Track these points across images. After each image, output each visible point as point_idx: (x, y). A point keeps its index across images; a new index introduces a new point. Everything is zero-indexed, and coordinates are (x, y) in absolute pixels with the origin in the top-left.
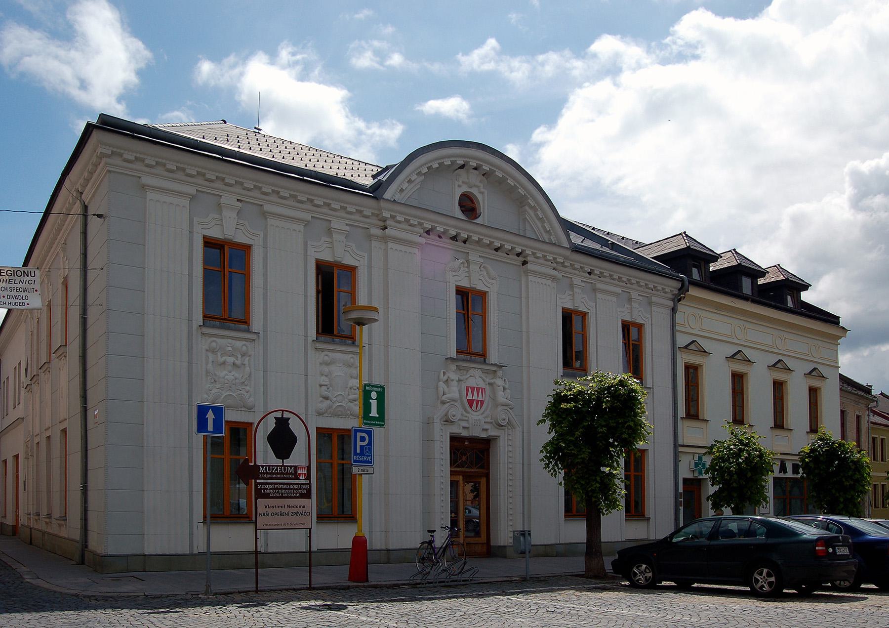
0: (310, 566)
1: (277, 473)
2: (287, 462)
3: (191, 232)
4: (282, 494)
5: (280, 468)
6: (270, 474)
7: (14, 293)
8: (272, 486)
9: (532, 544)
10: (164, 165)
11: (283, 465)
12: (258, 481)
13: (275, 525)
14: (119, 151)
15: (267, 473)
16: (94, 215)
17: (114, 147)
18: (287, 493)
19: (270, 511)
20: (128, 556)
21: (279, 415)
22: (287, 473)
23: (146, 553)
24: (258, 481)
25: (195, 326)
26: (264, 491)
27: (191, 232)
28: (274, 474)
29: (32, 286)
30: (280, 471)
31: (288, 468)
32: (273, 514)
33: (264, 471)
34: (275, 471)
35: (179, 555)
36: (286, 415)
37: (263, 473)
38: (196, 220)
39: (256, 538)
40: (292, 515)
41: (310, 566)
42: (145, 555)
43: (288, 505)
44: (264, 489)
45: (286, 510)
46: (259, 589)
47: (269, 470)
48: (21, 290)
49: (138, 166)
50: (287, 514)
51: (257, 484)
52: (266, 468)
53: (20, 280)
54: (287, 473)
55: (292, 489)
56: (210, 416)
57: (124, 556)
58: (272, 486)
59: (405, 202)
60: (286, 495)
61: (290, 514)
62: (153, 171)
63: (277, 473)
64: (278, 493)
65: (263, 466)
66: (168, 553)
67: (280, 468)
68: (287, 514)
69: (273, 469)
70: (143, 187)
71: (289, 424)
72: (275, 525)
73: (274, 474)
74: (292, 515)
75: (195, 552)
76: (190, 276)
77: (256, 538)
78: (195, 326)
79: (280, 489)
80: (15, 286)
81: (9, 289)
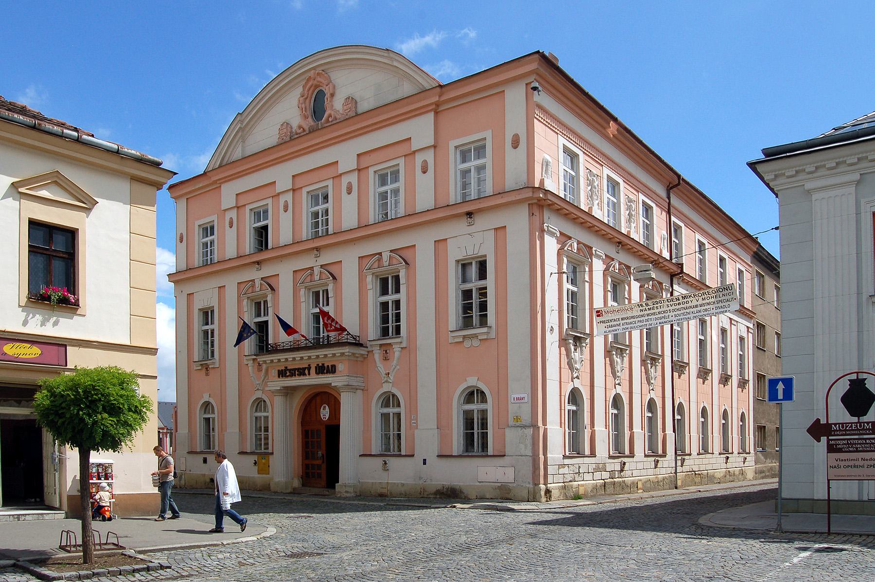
0: (829, 513)
1: (852, 430)
2: (865, 419)
3: (858, 213)
4: (857, 448)
5: (854, 425)
6: (861, 430)
7: (720, 304)
8: (845, 442)
9: (783, 497)
10: (824, 166)
11: (859, 422)
12: (830, 438)
13: (848, 476)
14: (780, 172)
15: (840, 430)
16: (773, 229)
17: (796, 167)
18: (863, 447)
19: (842, 464)
20: (798, 500)
21: (854, 377)
22: (863, 429)
23: (815, 498)
24: (830, 438)
25: (865, 297)
26: (836, 446)
27: (858, 213)
28: (848, 430)
29: (732, 296)
30: (854, 427)
31: (864, 425)
32: (845, 467)
33: (837, 428)
34: (849, 428)
35: (847, 501)
36: (861, 376)
37: (834, 431)
38: (863, 201)
39: (829, 488)
40: (867, 467)
41: (829, 513)
42: (813, 500)
43: (862, 459)
44: (836, 445)
45: (861, 463)
46: (831, 531)
47: (843, 427)
48: (725, 301)
49: (801, 176)
50: (863, 467)
51: (828, 440)
52: (839, 426)
53: (723, 294)
54: (863, 429)
55: (868, 444)
56: (780, 387)
57: (795, 499)
58: (845, 442)
59: (778, 191)
60: (861, 449)
61: (866, 466)
62: (815, 175)
63: (852, 430)
64: (852, 447)
65: (835, 424)
66: (836, 499)
67: (854, 425)
68: (863, 467)
69: (847, 427)
70: (809, 192)
71: (850, 385)
72: (848, 476)
73: (848, 430)
74: (867, 467)
75: (865, 498)
76: (859, 254)
77: (829, 488)
78: (865, 297)
79: (854, 444)
80: (720, 299)
81: (716, 303)
